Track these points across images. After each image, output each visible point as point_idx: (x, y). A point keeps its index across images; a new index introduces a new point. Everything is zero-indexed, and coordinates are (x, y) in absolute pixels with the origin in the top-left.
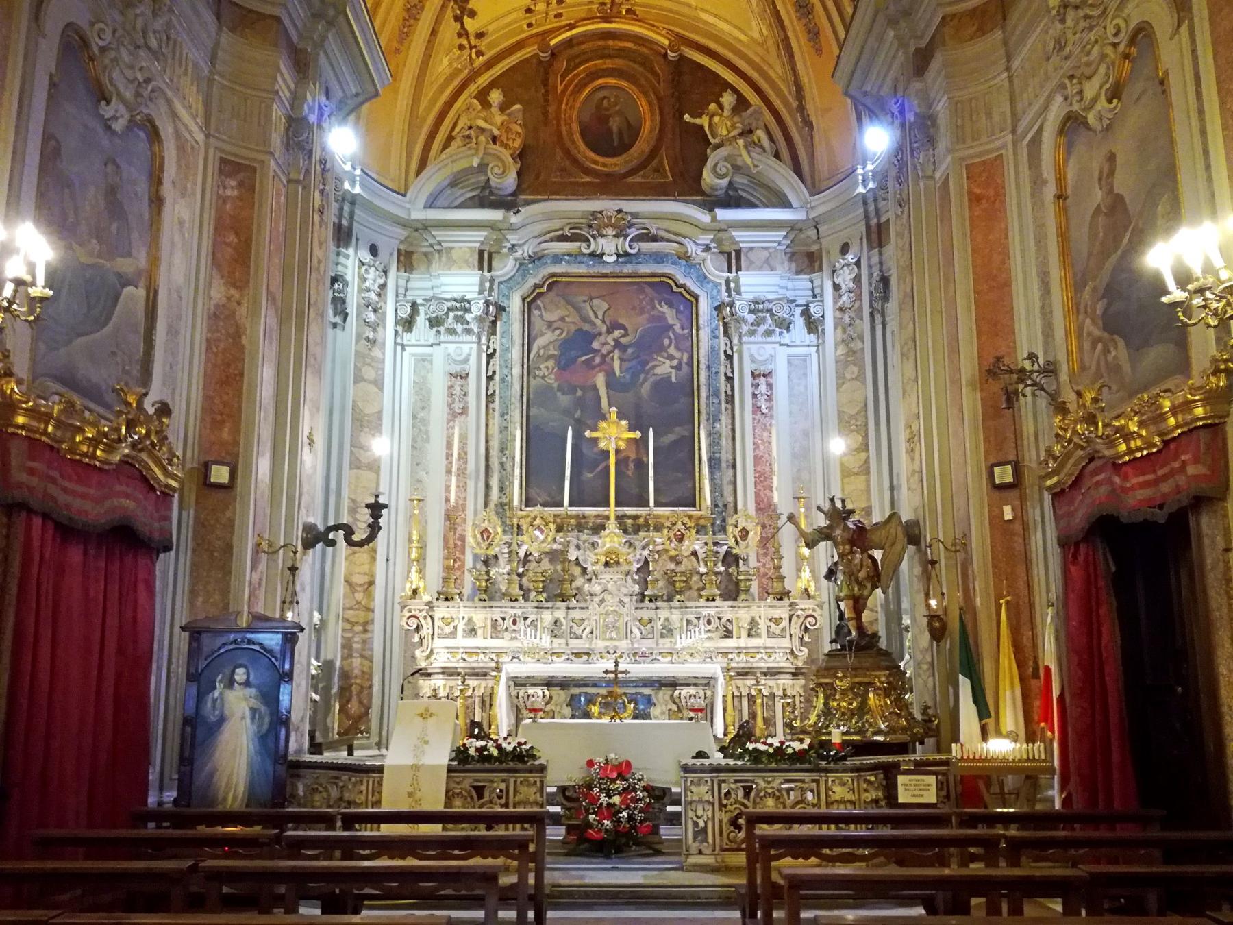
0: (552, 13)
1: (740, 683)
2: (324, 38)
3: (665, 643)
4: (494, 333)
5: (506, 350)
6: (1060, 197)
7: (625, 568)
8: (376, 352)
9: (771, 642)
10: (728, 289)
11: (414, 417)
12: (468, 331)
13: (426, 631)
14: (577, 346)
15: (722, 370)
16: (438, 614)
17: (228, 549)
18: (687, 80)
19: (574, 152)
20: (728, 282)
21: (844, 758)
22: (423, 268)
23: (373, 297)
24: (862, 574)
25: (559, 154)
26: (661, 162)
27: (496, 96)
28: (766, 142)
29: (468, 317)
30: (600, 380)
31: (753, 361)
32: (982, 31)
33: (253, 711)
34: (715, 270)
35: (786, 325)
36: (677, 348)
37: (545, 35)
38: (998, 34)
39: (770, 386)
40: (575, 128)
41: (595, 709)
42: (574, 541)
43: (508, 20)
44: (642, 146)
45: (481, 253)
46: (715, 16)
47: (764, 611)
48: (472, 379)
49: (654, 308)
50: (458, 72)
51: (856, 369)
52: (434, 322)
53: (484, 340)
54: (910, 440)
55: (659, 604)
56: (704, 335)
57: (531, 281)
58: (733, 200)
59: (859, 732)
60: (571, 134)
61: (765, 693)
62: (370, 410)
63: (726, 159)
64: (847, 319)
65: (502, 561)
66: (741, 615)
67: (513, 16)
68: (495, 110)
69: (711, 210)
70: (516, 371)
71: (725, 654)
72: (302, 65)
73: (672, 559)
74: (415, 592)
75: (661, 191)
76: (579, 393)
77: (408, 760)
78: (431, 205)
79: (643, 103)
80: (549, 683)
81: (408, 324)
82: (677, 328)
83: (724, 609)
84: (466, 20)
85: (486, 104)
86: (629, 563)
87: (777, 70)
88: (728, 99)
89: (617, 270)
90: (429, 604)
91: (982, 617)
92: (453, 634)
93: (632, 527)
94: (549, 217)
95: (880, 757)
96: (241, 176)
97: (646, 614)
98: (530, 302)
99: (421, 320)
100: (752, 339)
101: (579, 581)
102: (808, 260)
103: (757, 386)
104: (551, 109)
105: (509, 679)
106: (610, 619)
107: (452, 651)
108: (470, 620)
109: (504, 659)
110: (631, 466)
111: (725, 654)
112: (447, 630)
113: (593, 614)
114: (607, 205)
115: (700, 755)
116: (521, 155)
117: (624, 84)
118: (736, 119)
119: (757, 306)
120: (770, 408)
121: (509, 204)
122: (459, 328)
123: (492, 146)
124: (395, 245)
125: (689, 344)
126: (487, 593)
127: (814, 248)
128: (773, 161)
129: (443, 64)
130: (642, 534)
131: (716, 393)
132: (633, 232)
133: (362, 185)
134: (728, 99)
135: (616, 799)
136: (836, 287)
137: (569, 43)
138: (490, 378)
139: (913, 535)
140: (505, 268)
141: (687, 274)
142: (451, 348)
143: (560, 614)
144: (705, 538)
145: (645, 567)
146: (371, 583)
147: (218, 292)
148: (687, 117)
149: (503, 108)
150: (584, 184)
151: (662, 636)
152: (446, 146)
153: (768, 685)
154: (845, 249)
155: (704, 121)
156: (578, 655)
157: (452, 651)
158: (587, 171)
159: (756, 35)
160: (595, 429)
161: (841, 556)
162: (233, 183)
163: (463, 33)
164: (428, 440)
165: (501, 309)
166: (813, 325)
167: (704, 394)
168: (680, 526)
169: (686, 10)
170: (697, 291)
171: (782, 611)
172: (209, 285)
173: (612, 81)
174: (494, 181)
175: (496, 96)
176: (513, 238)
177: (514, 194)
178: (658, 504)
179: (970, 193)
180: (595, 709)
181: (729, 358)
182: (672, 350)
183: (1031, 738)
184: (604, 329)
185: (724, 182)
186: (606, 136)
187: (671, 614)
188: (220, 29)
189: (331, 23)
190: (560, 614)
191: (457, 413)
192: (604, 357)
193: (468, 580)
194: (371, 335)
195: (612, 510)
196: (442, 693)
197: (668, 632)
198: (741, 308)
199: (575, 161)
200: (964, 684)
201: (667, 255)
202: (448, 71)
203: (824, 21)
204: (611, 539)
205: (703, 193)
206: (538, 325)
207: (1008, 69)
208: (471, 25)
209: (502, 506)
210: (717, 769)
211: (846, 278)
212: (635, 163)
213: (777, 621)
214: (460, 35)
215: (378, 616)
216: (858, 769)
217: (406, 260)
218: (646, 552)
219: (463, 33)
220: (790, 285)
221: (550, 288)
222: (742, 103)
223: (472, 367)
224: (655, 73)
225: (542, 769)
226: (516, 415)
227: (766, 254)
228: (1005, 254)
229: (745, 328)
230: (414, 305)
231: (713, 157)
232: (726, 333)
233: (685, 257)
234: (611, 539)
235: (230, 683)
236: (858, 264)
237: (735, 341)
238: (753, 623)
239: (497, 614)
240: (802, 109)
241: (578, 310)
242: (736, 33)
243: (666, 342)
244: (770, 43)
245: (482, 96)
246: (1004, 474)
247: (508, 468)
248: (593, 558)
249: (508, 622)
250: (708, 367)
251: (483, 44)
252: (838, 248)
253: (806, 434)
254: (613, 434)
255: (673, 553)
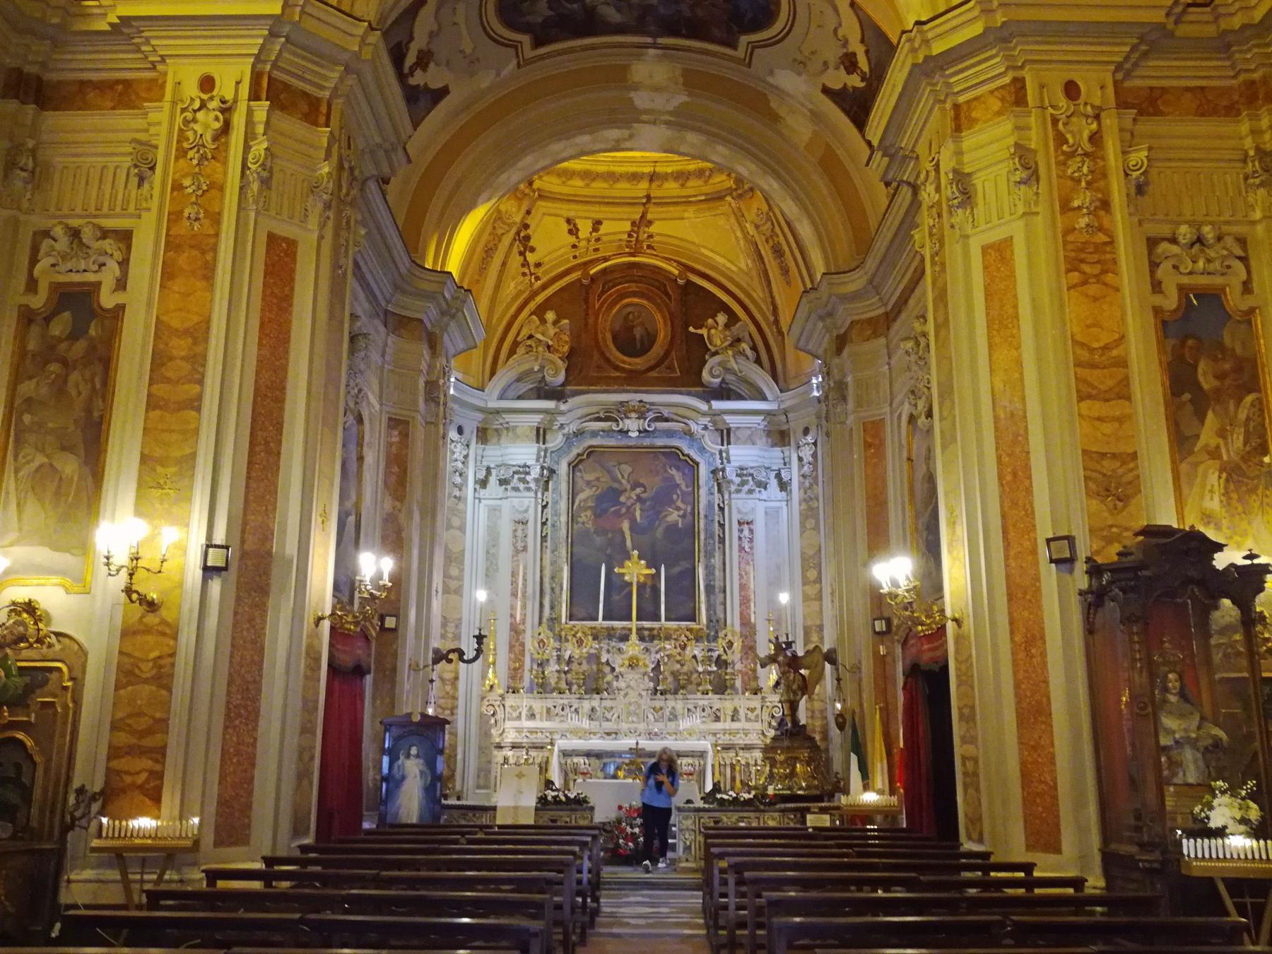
0: (591, 248)
1: (725, 755)
2: (447, 325)
3: (672, 725)
4: (546, 489)
5: (556, 503)
6: (909, 459)
7: (643, 670)
8: (461, 506)
9: (748, 725)
10: (721, 458)
11: (488, 552)
12: (529, 489)
13: (500, 715)
14: (608, 499)
15: (717, 518)
16: (508, 703)
17: (394, 670)
18: (691, 299)
19: (608, 355)
20: (721, 452)
21: (775, 804)
22: (494, 440)
23: (460, 465)
24: (795, 687)
25: (596, 355)
26: (672, 362)
27: (550, 316)
28: (749, 352)
29: (528, 478)
30: (626, 526)
31: (739, 512)
32: (876, 335)
33: (421, 772)
34: (711, 443)
35: (763, 485)
36: (683, 501)
37: (586, 265)
38: (883, 341)
39: (751, 531)
40: (609, 336)
41: (621, 774)
42: (606, 647)
43: (559, 253)
44: (657, 350)
45: (538, 429)
46: (712, 251)
47: (744, 702)
48: (531, 524)
49: (666, 471)
50: (520, 292)
51: (813, 521)
52: (503, 482)
53: (540, 495)
54: (832, 593)
55: (668, 696)
56: (703, 492)
57: (575, 451)
58: (724, 393)
59: (790, 788)
60: (605, 340)
61: (743, 762)
62: (456, 549)
63: (720, 364)
64: (807, 484)
65: (552, 662)
66: (726, 704)
67: (563, 250)
68: (549, 325)
69: (708, 402)
70: (563, 519)
71: (715, 734)
72: (433, 343)
73: (678, 662)
74: (492, 687)
75: (672, 384)
76: (610, 535)
77: (511, 803)
78: (501, 398)
79: (658, 317)
80: (588, 754)
81: (483, 483)
82: (683, 487)
83: (714, 700)
84: (528, 254)
85: (543, 321)
86: (646, 666)
87: (759, 294)
88: (722, 318)
89: (639, 443)
90: (502, 696)
91: (867, 717)
92: (519, 718)
93: (647, 637)
94: (589, 404)
95: (795, 802)
96: (400, 428)
97: (658, 704)
98: (574, 466)
99: (493, 480)
100: (739, 496)
101: (609, 677)
102: (781, 437)
103: (741, 531)
104: (591, 321)
105: (560, 751)
106: (632, 708)
107: (519, 730)
108: (531, 707)
109: (556, 736)
110: (648, 590)
111: (715, 734)
112: (515, 714)
113: (620, 703)
114: (632, 398)
115: (689, 802)
116: (569, 357)
117: (645, 302)
118: (727, 333)
119: (742, 472)
120: (751, 548)
121: (557, 394)
122: (521, 486)
123: (547, 353)
124: (475, 424)
125: (693, 499)
126: (542, 687)
127: (784, 427)
128: (756, 367)
129: (510, 288)
130: (656, 642)
131: (712, 537)
132: (651, 415)
133: (455, 388)
134: (722, 318)
135: (637, 830)
136: (800, 459)
137: (604, 271)
138: (544, 524)
139: (831, 657)
140: (556, 441)
141: (691, 446)
142: (516, 501)
143: (596, 703)
144: (701, 645)
145: (657, 668)
146: (456, 678)
147: (388, 505)
148: (691, 329)
149: (555, 323)
150: (616, 378)
151: (670, 720)
152: (512, 352)
153: (743, 757)
154: (806, 431)
155: (704, 332)
156: (608, 734)
157: (519, 730)
158: (617, 368)
159: (744, 267)
160: (622, 566)
161: (783, 673)
162: (396, 433)
163: (525, 264)
164: (497, 571)
165: (552, 472)
166: (783, 486)
167: (702, 537)
168: (683, 638)
169: (692, 247)
170: (698, 459)
171: (756, 702)
172: (383, 501)
173: (636, 300)
174: (548, 379)
175: (550, 316)
176: (561, 420)
177: (563, 385)
178: (667, 619)
179: (865, 442)
180: (621, 774)
181: (721, 509)
182: (679, 503)
183: (892, 792)
184: (629, 487)
185: (718, 380)
186: (630, 343)
187: (675, 703)
188: (388, 334)
189: (453, 317)
190: (596, 703)
191: (520, 550)
192: (628, 508)
193: (527, 677)
194: (458, 493)
195: (634, 624)
196: (511, 761)
197: (674, 717)
198: (730, 473)
199: (608, 360)
200: (854, 759)
201: (675, 432)
202: (514, 292)
203: (792, 265)
204: (633, 647)
205: (702, 385)
206: (580, 483)
207: (889, 364)
208: (531, 258)
209: (554, 620)
210: (698, 810)
211: (807, 453)
212: (653, 362)
213: (752, 710)
214: (523, 265)
215: (461, 702)
216: (783, 811)
217: (483, 435)
218: (658, 656)
219: (525, 264)
220: (766, 454)
221: (589, 455)
222: (733, 319)
223: (530, 516)
224: (667, 294)
225: (592, 809)
226: (563, 552)
227: (749, 432)
228: (885, 486)
229: (733, 488)
230: (488, 469)
231: (712, 362)
232: (720, 491)
233: (689, 434)
234: (633, 647)
235: (408, 756)
236: (815, 444)
237: (726, 496)
238: (736, 711)
239: (550, 704)
240: (777, 322)
241: (609, 472)
242: (728, 265)
243: (675, 497)
244: (754, 273)
245: (540, 312)
246: (880, 626)
247: (557, 590)
248: (620, 662)
249: (558, 709)
250: (706, 516)
251: (540, 272)
252: (801, 430)
253: (778, 568)
254: (635, 570)
255: (678, 658)
